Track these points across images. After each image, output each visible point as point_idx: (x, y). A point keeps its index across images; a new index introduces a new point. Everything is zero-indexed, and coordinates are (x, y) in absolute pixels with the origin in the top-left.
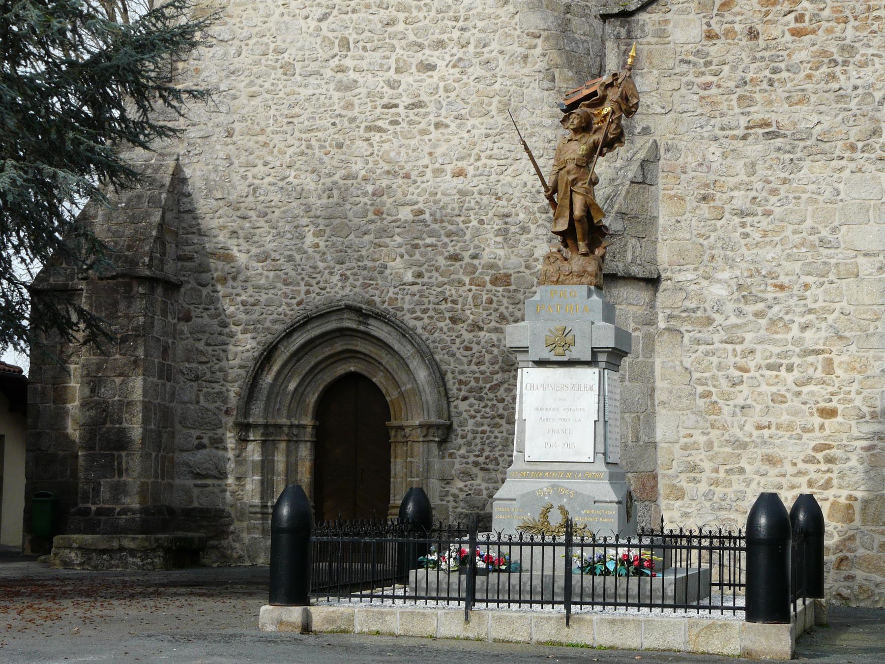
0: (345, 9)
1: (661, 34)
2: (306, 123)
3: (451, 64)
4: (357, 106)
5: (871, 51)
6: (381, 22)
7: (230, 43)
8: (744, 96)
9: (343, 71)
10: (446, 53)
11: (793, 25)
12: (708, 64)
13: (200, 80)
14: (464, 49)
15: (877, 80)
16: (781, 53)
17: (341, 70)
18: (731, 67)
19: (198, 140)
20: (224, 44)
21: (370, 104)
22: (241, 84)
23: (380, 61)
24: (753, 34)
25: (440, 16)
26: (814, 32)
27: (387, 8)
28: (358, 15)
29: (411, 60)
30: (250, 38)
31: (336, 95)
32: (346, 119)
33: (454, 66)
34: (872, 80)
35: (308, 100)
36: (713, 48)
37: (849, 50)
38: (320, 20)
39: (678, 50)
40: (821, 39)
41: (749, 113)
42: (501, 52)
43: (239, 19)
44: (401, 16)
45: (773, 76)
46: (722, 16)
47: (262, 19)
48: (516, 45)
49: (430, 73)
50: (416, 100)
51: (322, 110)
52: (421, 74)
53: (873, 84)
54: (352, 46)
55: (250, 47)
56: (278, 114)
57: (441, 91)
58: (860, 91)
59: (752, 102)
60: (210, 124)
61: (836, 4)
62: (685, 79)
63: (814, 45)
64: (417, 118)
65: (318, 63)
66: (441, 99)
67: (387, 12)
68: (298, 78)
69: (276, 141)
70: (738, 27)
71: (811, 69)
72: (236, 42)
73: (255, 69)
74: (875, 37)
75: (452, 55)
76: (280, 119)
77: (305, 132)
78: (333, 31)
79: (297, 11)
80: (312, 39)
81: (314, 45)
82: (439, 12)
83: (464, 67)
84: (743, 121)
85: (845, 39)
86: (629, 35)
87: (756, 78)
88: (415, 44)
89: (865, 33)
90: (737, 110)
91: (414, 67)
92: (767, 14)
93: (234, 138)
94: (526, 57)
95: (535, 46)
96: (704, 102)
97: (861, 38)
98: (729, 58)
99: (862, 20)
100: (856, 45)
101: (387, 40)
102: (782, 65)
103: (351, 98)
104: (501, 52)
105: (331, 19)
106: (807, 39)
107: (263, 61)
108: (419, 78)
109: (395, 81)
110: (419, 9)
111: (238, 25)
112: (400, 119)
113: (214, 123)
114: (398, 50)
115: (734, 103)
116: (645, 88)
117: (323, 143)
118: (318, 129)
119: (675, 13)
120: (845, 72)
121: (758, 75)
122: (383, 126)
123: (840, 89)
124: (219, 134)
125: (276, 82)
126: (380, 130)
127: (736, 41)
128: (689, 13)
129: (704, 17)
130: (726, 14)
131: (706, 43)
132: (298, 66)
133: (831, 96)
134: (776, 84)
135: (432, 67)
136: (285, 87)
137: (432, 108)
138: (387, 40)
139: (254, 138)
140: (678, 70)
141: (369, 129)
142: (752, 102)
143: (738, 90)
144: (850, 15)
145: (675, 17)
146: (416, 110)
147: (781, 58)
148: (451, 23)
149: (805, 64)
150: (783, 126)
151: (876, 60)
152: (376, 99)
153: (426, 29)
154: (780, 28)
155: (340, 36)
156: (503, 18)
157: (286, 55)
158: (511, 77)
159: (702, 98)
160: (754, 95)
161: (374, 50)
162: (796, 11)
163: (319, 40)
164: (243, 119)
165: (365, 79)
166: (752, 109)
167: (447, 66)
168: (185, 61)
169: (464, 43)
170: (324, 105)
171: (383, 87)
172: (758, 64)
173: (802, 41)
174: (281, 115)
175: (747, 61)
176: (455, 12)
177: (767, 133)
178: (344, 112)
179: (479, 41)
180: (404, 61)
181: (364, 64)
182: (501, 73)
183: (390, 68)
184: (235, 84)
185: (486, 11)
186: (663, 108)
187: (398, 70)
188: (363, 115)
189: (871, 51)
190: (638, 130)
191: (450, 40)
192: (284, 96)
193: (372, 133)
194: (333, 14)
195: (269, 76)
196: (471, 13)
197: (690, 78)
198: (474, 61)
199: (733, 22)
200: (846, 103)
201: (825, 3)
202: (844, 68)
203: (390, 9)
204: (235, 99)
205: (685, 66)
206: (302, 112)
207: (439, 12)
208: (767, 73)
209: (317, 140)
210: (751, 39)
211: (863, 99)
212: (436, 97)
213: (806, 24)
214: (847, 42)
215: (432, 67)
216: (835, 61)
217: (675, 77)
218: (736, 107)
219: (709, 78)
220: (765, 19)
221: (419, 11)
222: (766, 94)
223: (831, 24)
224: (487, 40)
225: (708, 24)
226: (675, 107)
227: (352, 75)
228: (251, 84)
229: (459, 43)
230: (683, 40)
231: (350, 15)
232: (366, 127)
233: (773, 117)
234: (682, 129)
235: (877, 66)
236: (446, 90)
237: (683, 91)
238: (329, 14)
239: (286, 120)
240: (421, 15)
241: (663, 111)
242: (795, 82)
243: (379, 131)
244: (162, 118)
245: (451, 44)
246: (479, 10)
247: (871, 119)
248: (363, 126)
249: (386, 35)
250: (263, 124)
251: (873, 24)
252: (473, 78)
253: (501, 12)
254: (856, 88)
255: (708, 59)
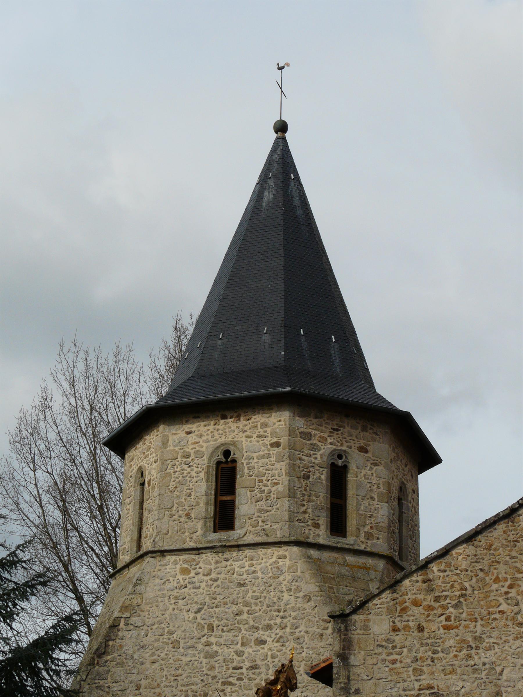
0: (212, 605)
1: (366, 628)
2: (185, 680)
3: (276, 640)
4: (217, 669)
5: (492, 640)
6: (233, 613)
7: (141, 628)
8: (417, 668)
9: (209, 645)
10: (272, 633)
11: (444, 623)
12: (394, 647)
13: (122, 652)
14: (284, 630)
15: (497, 659)
16: (438, 641)
17: (208, 644)
18: (408, 650)
19: (119, 692)
20: (138, 628)
21: (225, 667)
22: (147, 655)
23: (232, 638)
24: (420, 629)
25: (269, 609)
26: (457, 627)
27: (237, 604)
28: (219, 609)
29: (251, 637)
30: (153, 625)
31: (204, 661)
32: (210, 677)
33: (277, 641)
34: (494, 659)
35: (187, 664)
36: (397, 637)
37: (479, 639)
38: (196, 613)
39: (376, 638)
40: (462, 632)
41: (420, 679)
42: (306, 632)
43: (148, 613)
44: (246, 609)
45: (433, 656)
46: (402, 617)
47: (161, 612)
48: (316, 627)
49: (263, 646)
50: (254, 664)
51: (195, 671)
52: (257, 647)
53: (495, 662)
54: (215, 628)
55: (153, 630)
56: (168, 674)
57: (269, 658)
58: (487, 666)
59: (422, 673)
60: (127, 681)
61: (469, 610)
62: (381, 657)
63: (457, 636)
64: (254, 676)
65: (194, 640)
66: (269, 663)
67: (237, 607)
68: (182, 650)
69: (166, 692)
70: (411, 624)
71: (456, 651)
72: (145, 628)
73: (156, 645)
74: (494, 631)
75: (276, 634)
76: (169, 677)
77: (184, 686)
78: (204, 619)
79: (183, 607)
80: (191, 625)
81: (192, 629)
82: (268, 606)
83: (284, 642)
84: (417, 685)
85: (476, 632)
86: (346, 630)
87: (424, 657)
88: (253, 627)
89: (488, 629)
90: (413, 678)
91: (253, 642)
92: (428, 616)
93: (141, 690)
94: (321, 635)
95: (327, 628)
96: (392, 673)
97: (486, 632)
98: (407, 644)
99: (485, 621)
100: (483, 636)
101: (237, 625)
102: (439, 649)
103: (214, 663)
104: (306, 632)
105: (203, 612)
106: (453, 632)
107: (161, 640)
108: (256, 649)
109: (241, 651)
110: (256, 604)
111: (147, 616)
112: (243, 677)
113: (129, 680)
114: (243, 631)
115: (411, 673)
116: (356, 663)
117: (195, 693)
118: (193, 684)
119: (373, 615)
120: (477, 654)
121: (425, 655)
122: (233, 681)
123: (475, 665)
124: (132, 688)
125: (168, 653)
126: (231, 684)
127: (411, 633)
128: (382, 615)
129: (391, 617)
130: (404, 616)
131: (392, 634)
132: (182, 642)
133: (469, 669)
134: (436, 661)
135: (264, 642)
136: (173, 656)
137: (263, 669)
138: (237, 625)
139: (153, 690)
140: (376, 651)
141: (224, 683)
142: (422, 673)
143: (413, 664)
144: (478, 617)
145: (374, 617)
146: (253, 671)
147: (438, 644)
148: (276, 614)
149: (453, 648)
150: (441, 689)
151: (496, 646)
152: (229, 663)
153: (260, 617)
154: (437, 625)
155: (208, 622)
156: (308, 610)
157: (175, 635)
158: (312, 649)
159: (391, 670)
160: (423, 668)
161: (228, 632)
162: (445, 614)
163: (195, 625)
164: (147, 678)
165: (222, 650)
166: (422, 677)
167: (273, 641)
168: (113, 640)
169: (283, 626)
170: (197, 667)
171: (233, 656)
172: (424, 647)
173: (450, 634)
174: (170, 675)
175: (418, 646)
176: (278, 607)
177: (432, 693)
178: (209, 673)
179: (293, 625)
180: (247, 638)
181: (222, 640)
182: (307, 646)
183: (238, 643)
184: (143, 654)
185: (297, 606)
186: (367, 676)
187: (243, 645)
188: (221, 674)
189: (492, 640)
190: (353, 690)
191: (275, 624)
192: (173, 662)
193: (226, 686)
194: (204, 609)
195: (163, 648)
196: (288, 607)
197: (384, 656)
198: (290, 638)
199: (408, 621)
200: (479, 674)
201: (463, 609)
202: (477, 651)
203: (239, 605)
204: (143, 664)
205: (380, 648)
206: (183, 672)
207: (268, 606)
208: (430, 653)
209: (192, 692)
210: (419, 632)
211: (489, 672)
212: (266, 662)
213: (452, 622)
214: (477, 634)
215: (264, 642)
216: (471, 646)
217: (375, 656)
218: (412, 676)
219: (395, 657)
220: (428, 619)
221: (256, 606)
222: (430, 667)
223: (467, 622)
224: (298, 624)
225: (394, 622)
226: (375, 675)
227: (215, 648)
228: (153, 654)
229: (280, 626)
230: (378, 632)
231: (214, 609)
232: (222, 682)
233: (435, 683)
234: (379, 690)
235: (497, 650)
236: (272, 657)
237: (380, 665)
238: (202, 608)
239: (173, 678)
240: (257, 608)
241: (368, 678)
242: (447, 660)
243: (230, 685)
244: (97, 678)
245: (276, 627)
246: (293, 605)
247: (495, 685)
248: (220, 681)
249: (236, 622)
250: (159, 681)
251: (492, 623)
252: (289, 649)
253: (306, 606)
254: (484, 664)
255: (394, 644)
